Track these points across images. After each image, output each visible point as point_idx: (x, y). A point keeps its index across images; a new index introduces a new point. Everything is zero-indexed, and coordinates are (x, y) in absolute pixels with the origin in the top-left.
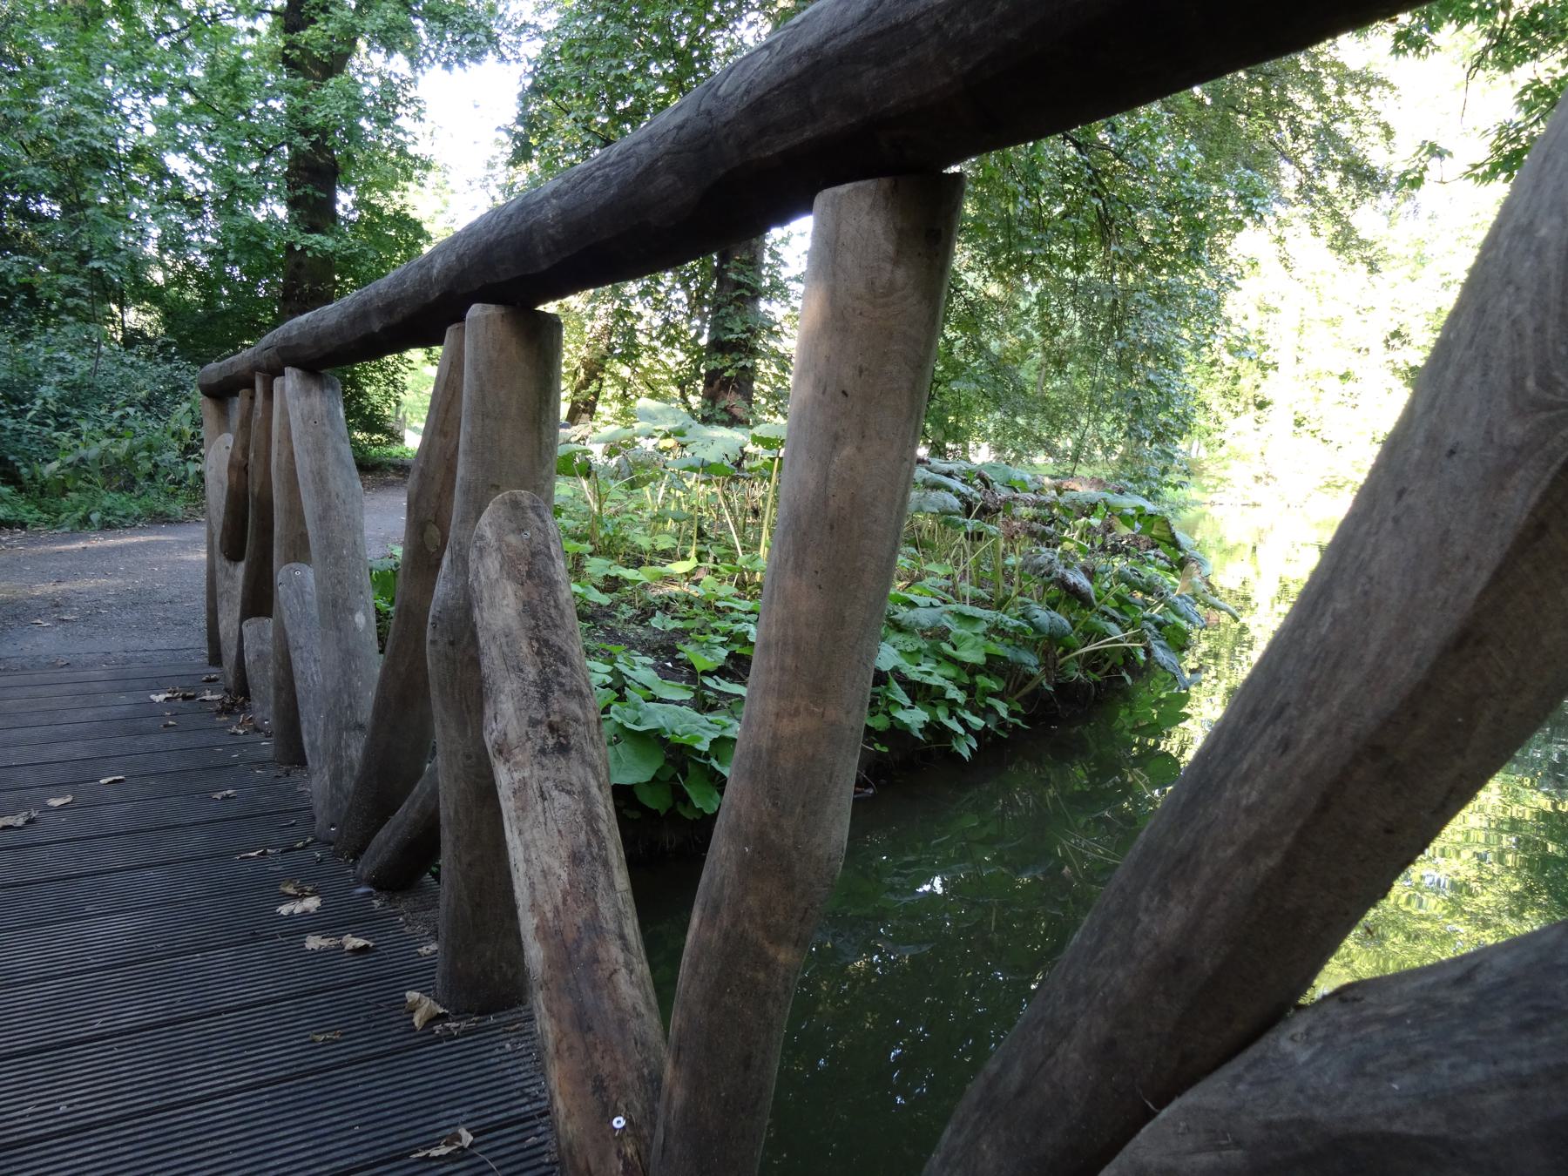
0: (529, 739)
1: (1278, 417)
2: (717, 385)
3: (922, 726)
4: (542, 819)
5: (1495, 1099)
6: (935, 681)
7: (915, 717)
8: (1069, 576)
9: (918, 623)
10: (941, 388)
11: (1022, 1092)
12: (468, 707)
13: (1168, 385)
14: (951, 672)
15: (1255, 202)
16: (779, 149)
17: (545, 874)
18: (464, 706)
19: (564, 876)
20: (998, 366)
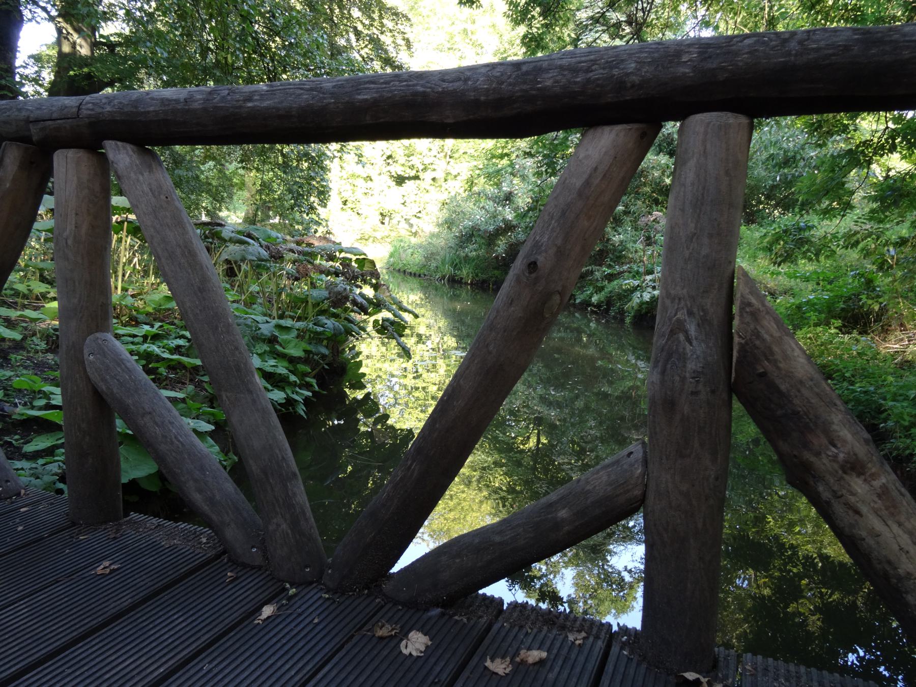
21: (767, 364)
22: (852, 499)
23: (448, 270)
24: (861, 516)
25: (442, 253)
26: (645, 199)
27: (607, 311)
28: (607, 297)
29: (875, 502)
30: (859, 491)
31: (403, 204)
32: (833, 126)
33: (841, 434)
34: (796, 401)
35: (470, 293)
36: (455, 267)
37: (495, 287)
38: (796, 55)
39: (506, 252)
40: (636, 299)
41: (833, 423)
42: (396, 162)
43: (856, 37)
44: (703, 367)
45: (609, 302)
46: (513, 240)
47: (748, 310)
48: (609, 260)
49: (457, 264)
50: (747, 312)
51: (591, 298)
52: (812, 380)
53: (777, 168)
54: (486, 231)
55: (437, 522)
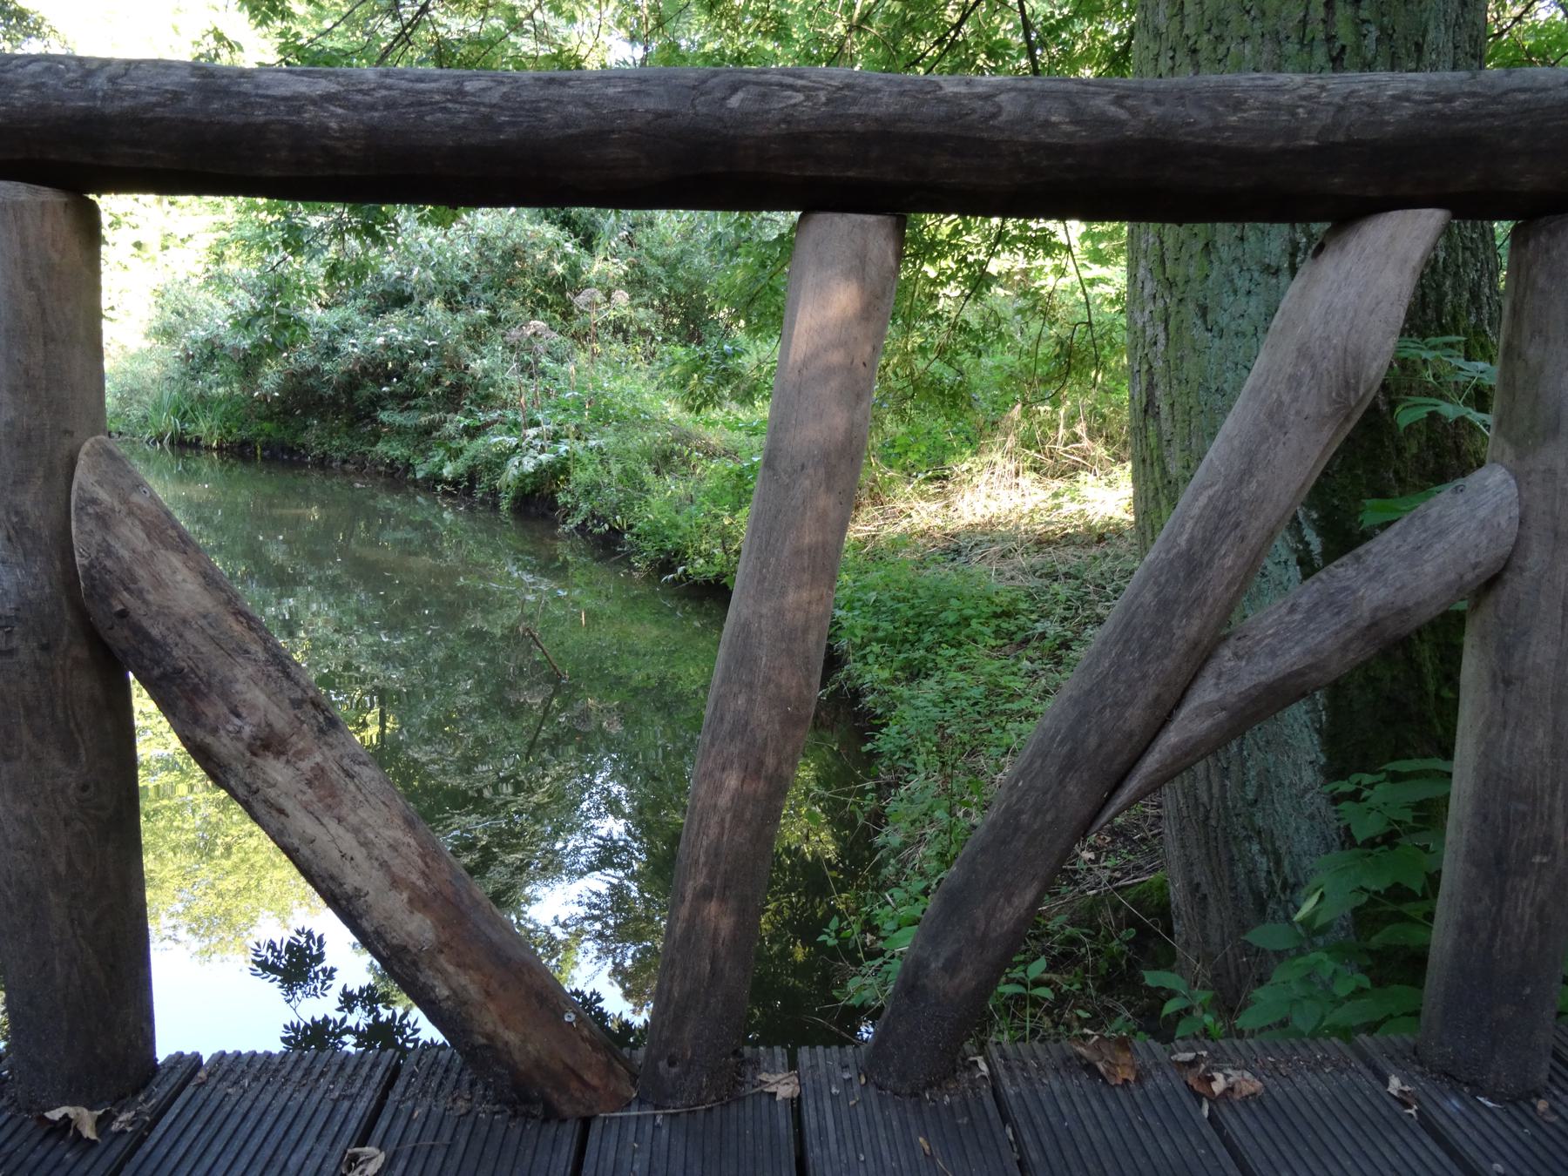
0: (302, 722)
2: (280, 288)
4: (360, 797)
5: (1329, 642)
11: (1100, 746)
12: (77, 725)
16: (808, 173)
17: (393, 847)
18: (72, 725)
19: (413, 842)
21: (128, 596)
22: (272, 793)
23: (168, 423)
24: (287, 816)
26: (525, 298)
27: (469, 491)
28: (469, 467)
29: (304, 793)
30: (280, 779)
33: (248, 696)
34: (176, 652)
35: (217, 464)
37: (266, 453)
38: (104, 99)
39: (280, 388)
40: (511, 471)
41: (237, 681)
43: (193, 80)
44: (17, 609)
45: (472, 476)
46: (294, 366)
47: (90, 510)
48: (468, 402)
49: (185, 413)
50: (88, 514)
51: (441, 468)
52: (205, 617)
53: (728, 255)
54: (235, 349)
55: (201, 903)
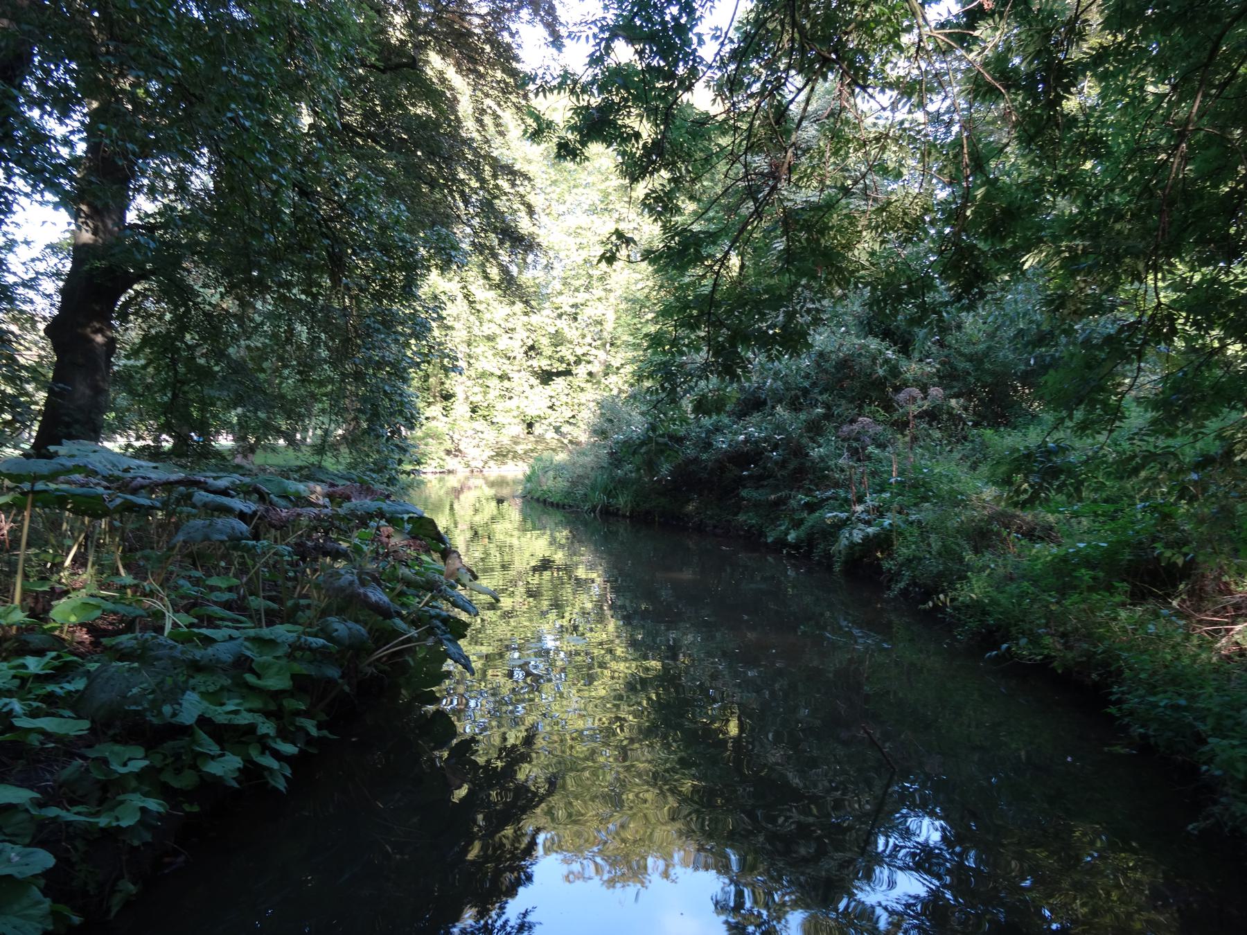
1: (460, 408)
3: (236, 775)
6: (245, 719)
7: (226, 766)
8: (370, 595)
9: (218, 661)
10: (186, 388)
13: (401, 395)
14: (257, 704)
15: (453, 253)
20: (237, 368)
23: (599, 498)
25: (592, 474)
27: (810, 552)
31: (551, 407)
32: (1083, 303)
36: (609, 494)
42: (541, 354)
45: (809, 542)
51: (787, 534)
53: (1030, 348)
